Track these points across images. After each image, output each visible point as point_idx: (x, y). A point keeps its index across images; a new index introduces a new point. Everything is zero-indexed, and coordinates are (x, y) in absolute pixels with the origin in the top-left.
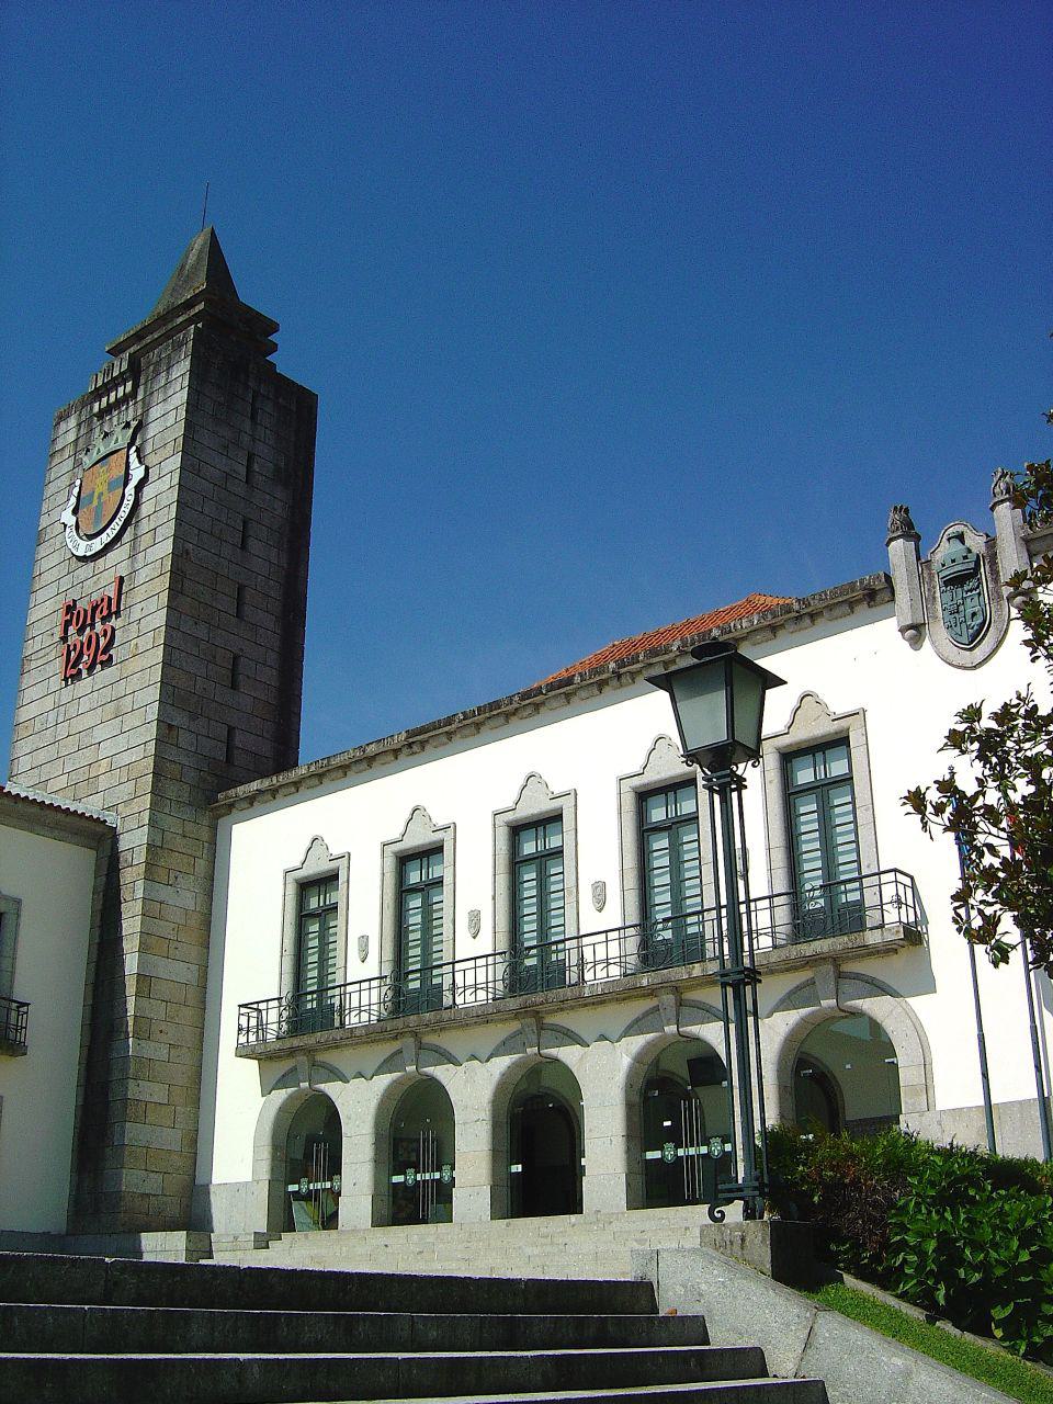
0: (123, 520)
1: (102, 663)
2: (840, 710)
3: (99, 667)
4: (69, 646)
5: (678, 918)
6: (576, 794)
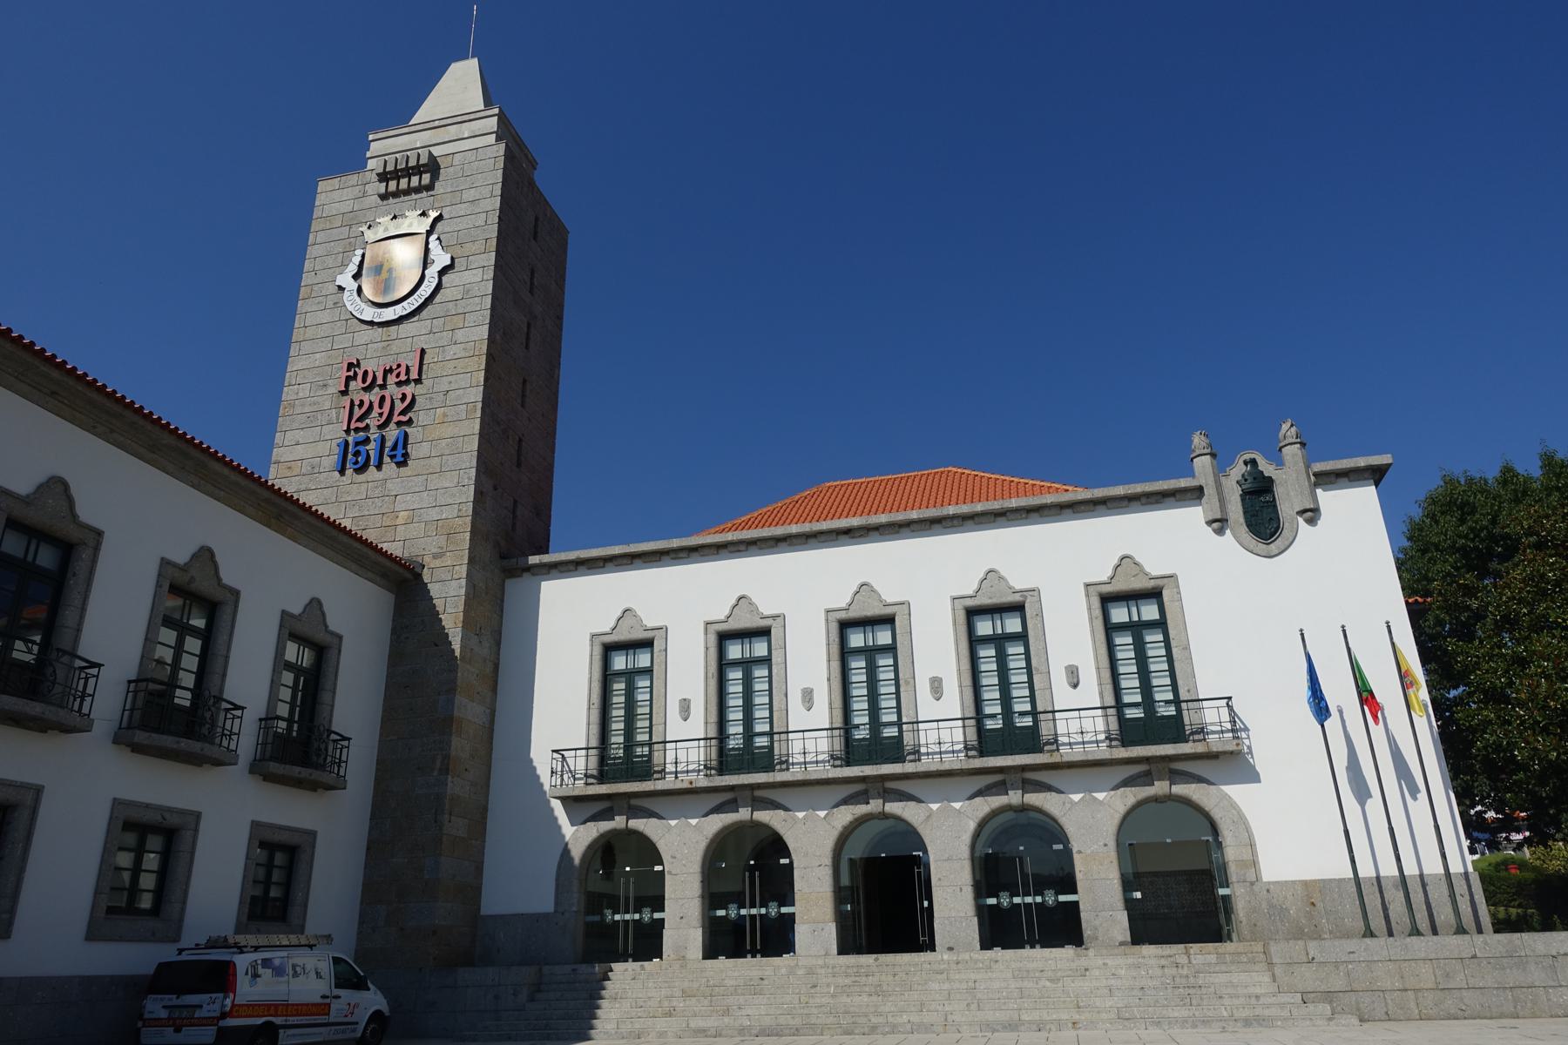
2: (650, 625)
4: (352, 401)
5: (749, 734)
6: (667, 629)
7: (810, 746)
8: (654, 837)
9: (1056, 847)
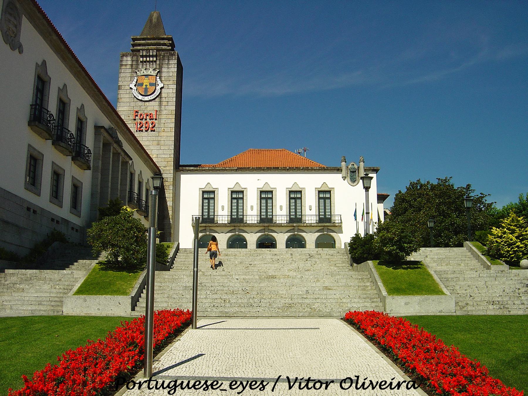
3: (150, 130)
5: (267, 215)
7: (224, 218)
8: (245, 236)
9: (244, 243)
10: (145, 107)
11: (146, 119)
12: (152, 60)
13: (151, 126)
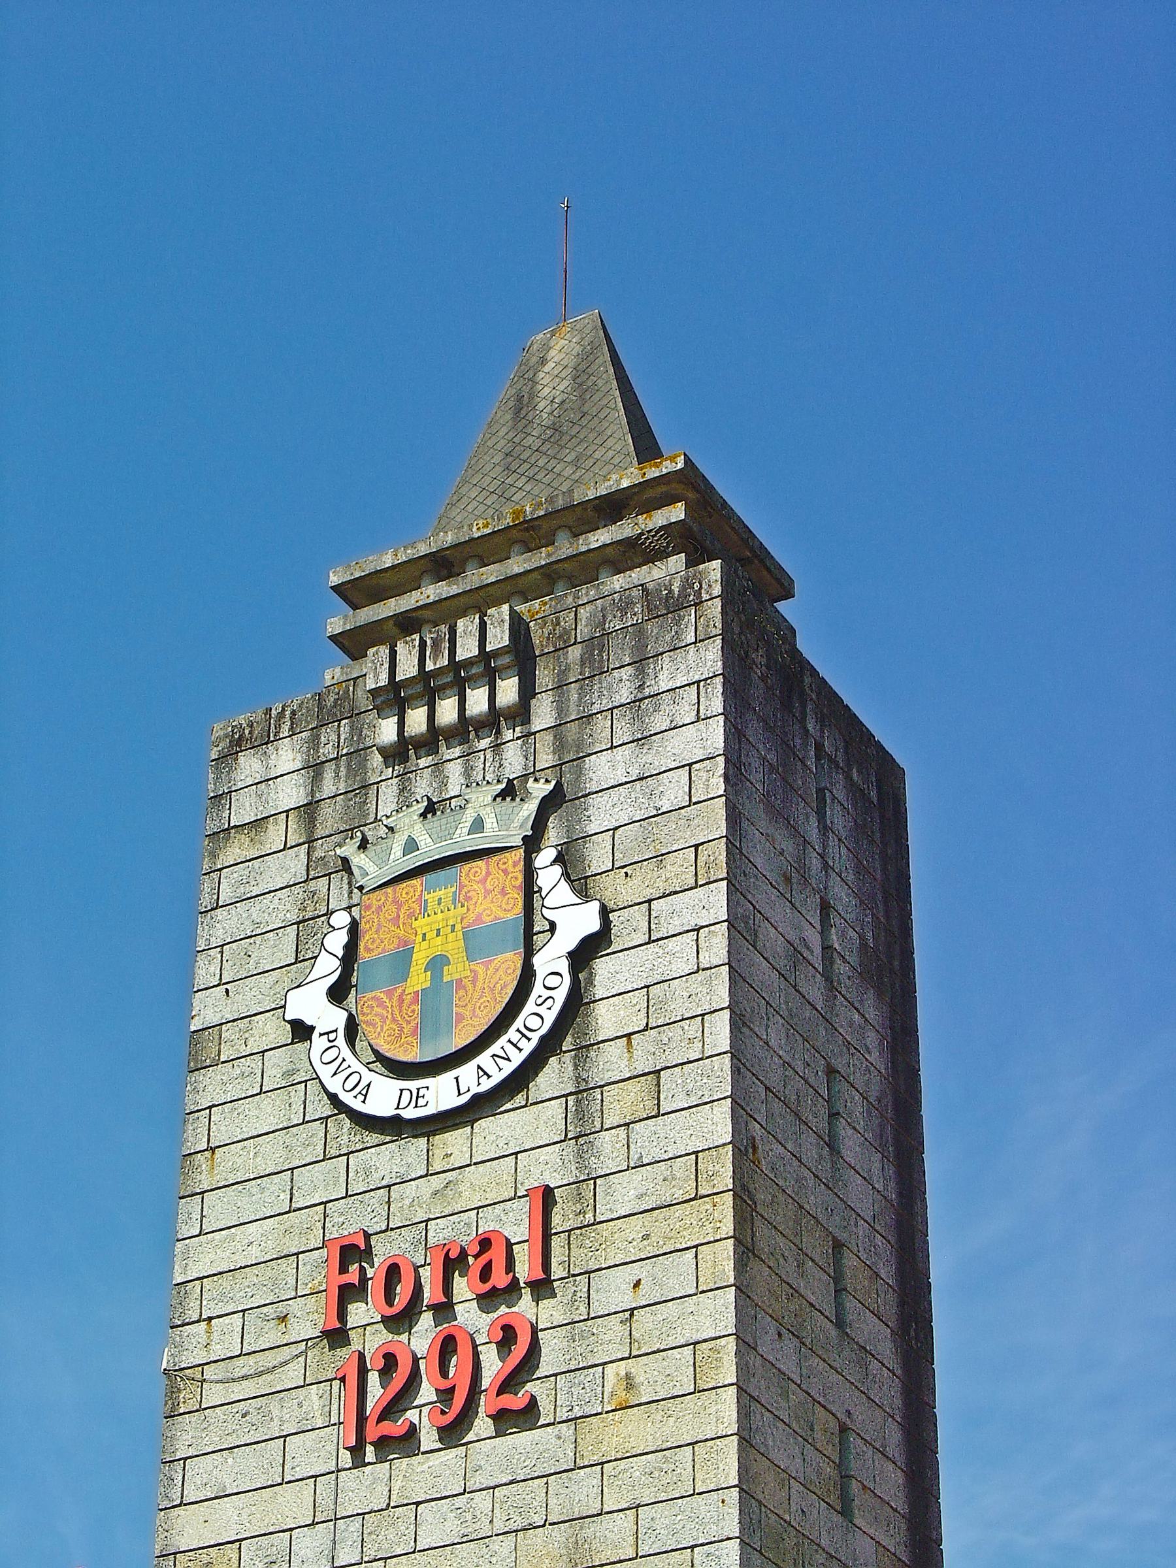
0: (535, 1037)
1: (383, 1444)
3: (482, 1425)
10: (436, 1182)
11: (444, 1309)
12: (485, 707)
13: (493, 1366)
